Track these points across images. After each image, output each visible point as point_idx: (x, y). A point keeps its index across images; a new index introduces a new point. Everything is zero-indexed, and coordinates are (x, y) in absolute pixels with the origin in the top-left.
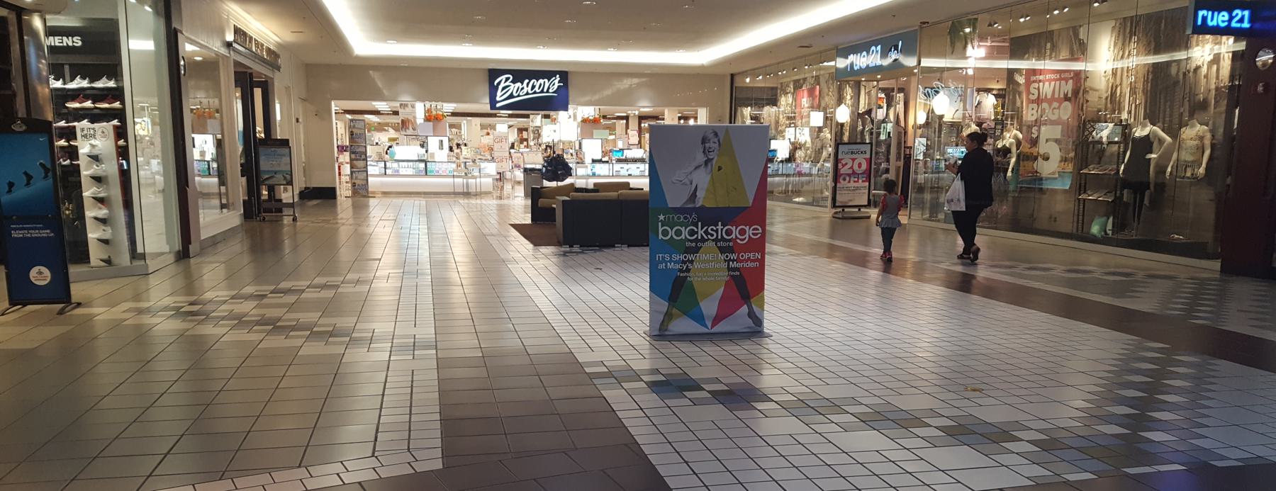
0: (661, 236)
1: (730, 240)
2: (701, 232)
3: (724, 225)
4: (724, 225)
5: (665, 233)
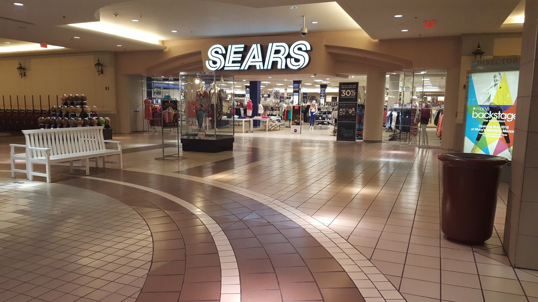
0: (473, 117)
1: (503, 120)
2: (491, 115)
3: (501, 113)
4: (501, 113)
5: (475, 115)
